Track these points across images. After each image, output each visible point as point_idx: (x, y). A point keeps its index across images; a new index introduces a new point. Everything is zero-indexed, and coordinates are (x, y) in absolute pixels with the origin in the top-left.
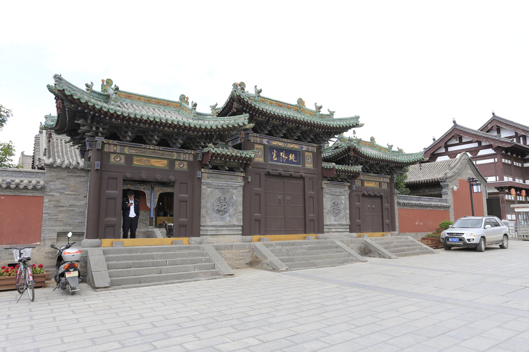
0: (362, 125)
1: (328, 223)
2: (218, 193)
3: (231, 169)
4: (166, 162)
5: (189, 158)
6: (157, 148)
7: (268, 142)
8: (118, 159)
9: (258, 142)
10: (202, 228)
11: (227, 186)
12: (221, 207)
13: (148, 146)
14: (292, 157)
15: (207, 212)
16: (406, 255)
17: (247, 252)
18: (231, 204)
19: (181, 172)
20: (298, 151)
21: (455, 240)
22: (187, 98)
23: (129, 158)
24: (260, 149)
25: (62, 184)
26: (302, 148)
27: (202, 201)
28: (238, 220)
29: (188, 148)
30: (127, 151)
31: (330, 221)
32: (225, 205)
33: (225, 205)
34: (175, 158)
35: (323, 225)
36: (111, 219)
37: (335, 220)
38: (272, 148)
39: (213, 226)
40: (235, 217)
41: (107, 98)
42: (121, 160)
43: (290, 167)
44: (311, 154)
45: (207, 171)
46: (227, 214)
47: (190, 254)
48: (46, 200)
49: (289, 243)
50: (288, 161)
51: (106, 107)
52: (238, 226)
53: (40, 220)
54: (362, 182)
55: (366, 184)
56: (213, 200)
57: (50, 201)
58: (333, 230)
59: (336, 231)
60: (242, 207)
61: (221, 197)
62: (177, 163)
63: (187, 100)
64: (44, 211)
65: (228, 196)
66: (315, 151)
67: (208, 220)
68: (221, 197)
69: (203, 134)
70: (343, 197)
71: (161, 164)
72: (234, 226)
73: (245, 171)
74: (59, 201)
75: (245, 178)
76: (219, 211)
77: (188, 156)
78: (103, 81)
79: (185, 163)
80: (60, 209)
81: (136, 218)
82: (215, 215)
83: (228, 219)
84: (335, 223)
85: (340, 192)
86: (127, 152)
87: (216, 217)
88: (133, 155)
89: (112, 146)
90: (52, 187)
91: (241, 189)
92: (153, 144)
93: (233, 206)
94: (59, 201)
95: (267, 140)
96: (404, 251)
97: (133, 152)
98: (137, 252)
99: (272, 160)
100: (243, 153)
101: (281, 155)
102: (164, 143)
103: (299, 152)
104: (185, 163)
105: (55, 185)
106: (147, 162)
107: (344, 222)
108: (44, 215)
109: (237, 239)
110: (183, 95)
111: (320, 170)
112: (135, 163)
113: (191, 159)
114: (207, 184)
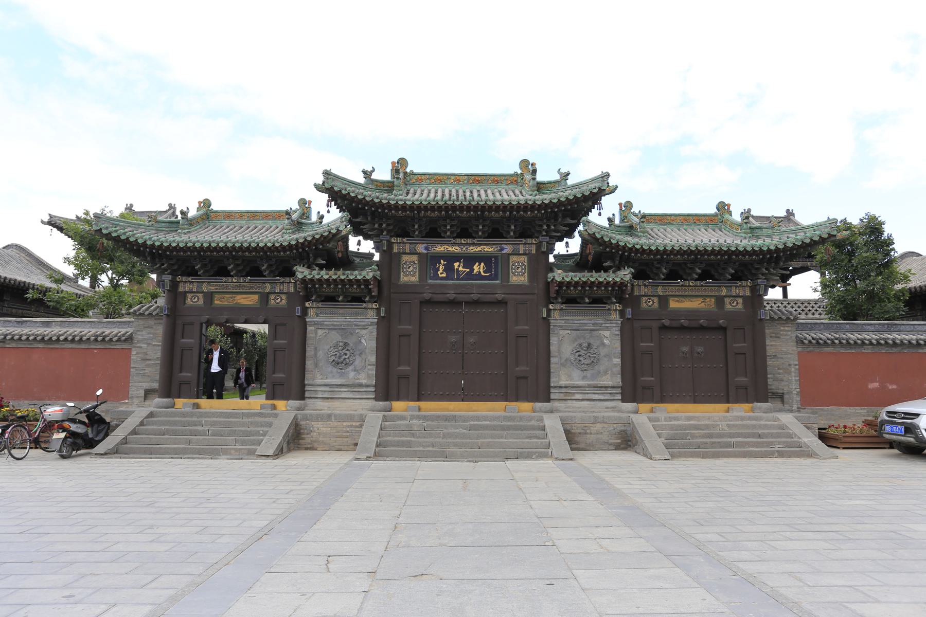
0: (617, 187)
1: (563, 383)
2: (335, 337)
3: (596, 301)
4: (256, 297)
6: (698, 283)
7: (426, 249)
9: (407, 251)
10: (307, 388)
11: (348, 325)
12: (340, 357)
13: (686, 283)
15: (316, 365)
16: (744, 455)
18: (358, 352)
19: (734, 315)
21: (897, 429)
22: (729, 205)
23: (209, 297)
24: (413, 261)
26: (502, 249)
28: (369, 376)
29: (740, 279)
31: (570, 377)
34: (268, 290)
35: (549, 387)
36: (186, 375)
37: (584, 378)
38: (436, 258)
40: (365, 370)
41: (630, 229)
42: (199, 300)
43: (472, 285)
44: (524, 259)
46: (351, 368)
47: (251, 423)
48: (134, 353)
49: (438, 417)
50: (470, 276)
51: (630, 241)
52: (367, 386)
53: (127, 376)
55: (673, 304)
56: (328, 347)
57: (137, 353)
58: (578, 396)
61: (342, 342)
65: (351, 341)
66: (534, 252)
68: (342, 342)
69: (696, 258)
70: (607, 333)
72: (361, 385)
74: (146, 354)
75: (622, 313)
77: (286, 286)
79: (284, 297)
80: (148, 362)
81: (221, 375)
82: (330, 368)
83: (352, 374)
84: (581, 383)
85: (594, 324)
86: (205, 290)
87: (332, 372)
92: (692, 279)
93: (360, 354)
94: (146, 354)
95: (424, 246)
96: (728, 445)
97: (212, 288)
98: (192, 417)
99: (436, 277)
102: (255, 272)
103: (496, 258)
107: (607, 381)
109: (363, 404)
111: (541, 285)
112: (216, 302)
113: (748, 293)
114: (316, 324)
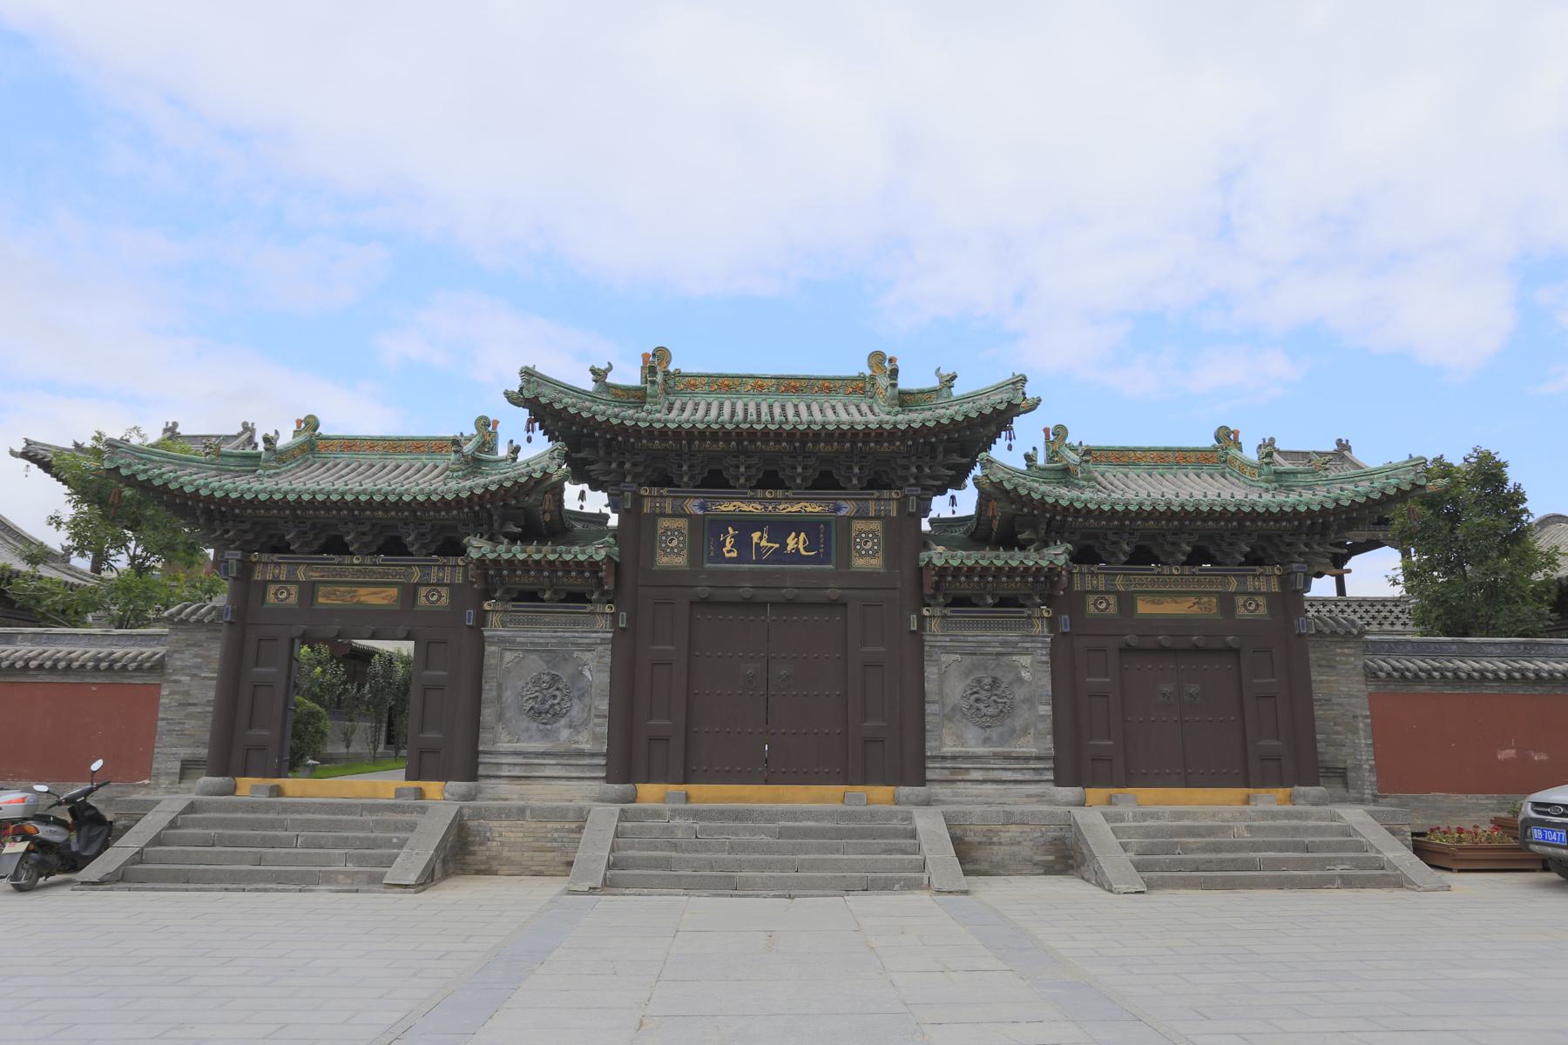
1: (948, 750)
2: (536, 664)
4: (394, 591)
5: (453, 577)
7: (703, 507)
8: (1103, 606)
11: (559, 644)
12: (544, 702)
13: (1166, 570)
14: (795, 542)
17: (571, 831)
18: (576, 693)
22: (1236, 433)
24: (678, 530)
25: (196, 656)
26: (838, 509)
27: (486, 687)
28: (595, 738)
30: (1120, 584)
31: (960, 739)
32: (555, 697)
33: (555, 697)
37: (986, 741)
39: (516, 754)
40: (587, 729)
41: (1064, 474)
42: (290, 597)
45: (938, 611)
46: (563, 722)
47: (377, 823)
48: (165, 692)
49: (722, 812)
51: (1066, 495)
52: (593, 755)
53: (150, 734)
55: (1144, 608)
56: (520, 684)
57: (172, 693)
59: (545, 773)
60: (607, 701)
63: (1236, 438)
64: (161, 715)
65: (565, 673)
66: (894, 513)
67: (504, 737)
68: (550, 677)
70: (1026, 660)
72: (580, 754)
73: (1049, 600)
74: (187, 693)
75: (1053, 624)
76: (536, 714)
77: (449, 572)
78: (1046, 431)
80: (191, 709)
83: (565, 734)
84: (980, 750)
86: (302, 578)
87: (528, 729)
88: (314, 582)
89: (270, 567)
90: (178, 663)
91: (605, 652)
93: (581, 697)
94: (187, 693)
96: (1251, 865)
97: (315, 576)
98: (267, 812)
99: (720, 557)
100: (968, 557)
101: (755, 540)
102: (394, 547)
103: (827, 524)
104: (444, 591)
105: (183, 660)
106: (348, 597)
107: (1026, 746)
108: (160, 723)
110: (481, 418)
112: (321, 600)
113: (1275, 588)
114: (501, 641)
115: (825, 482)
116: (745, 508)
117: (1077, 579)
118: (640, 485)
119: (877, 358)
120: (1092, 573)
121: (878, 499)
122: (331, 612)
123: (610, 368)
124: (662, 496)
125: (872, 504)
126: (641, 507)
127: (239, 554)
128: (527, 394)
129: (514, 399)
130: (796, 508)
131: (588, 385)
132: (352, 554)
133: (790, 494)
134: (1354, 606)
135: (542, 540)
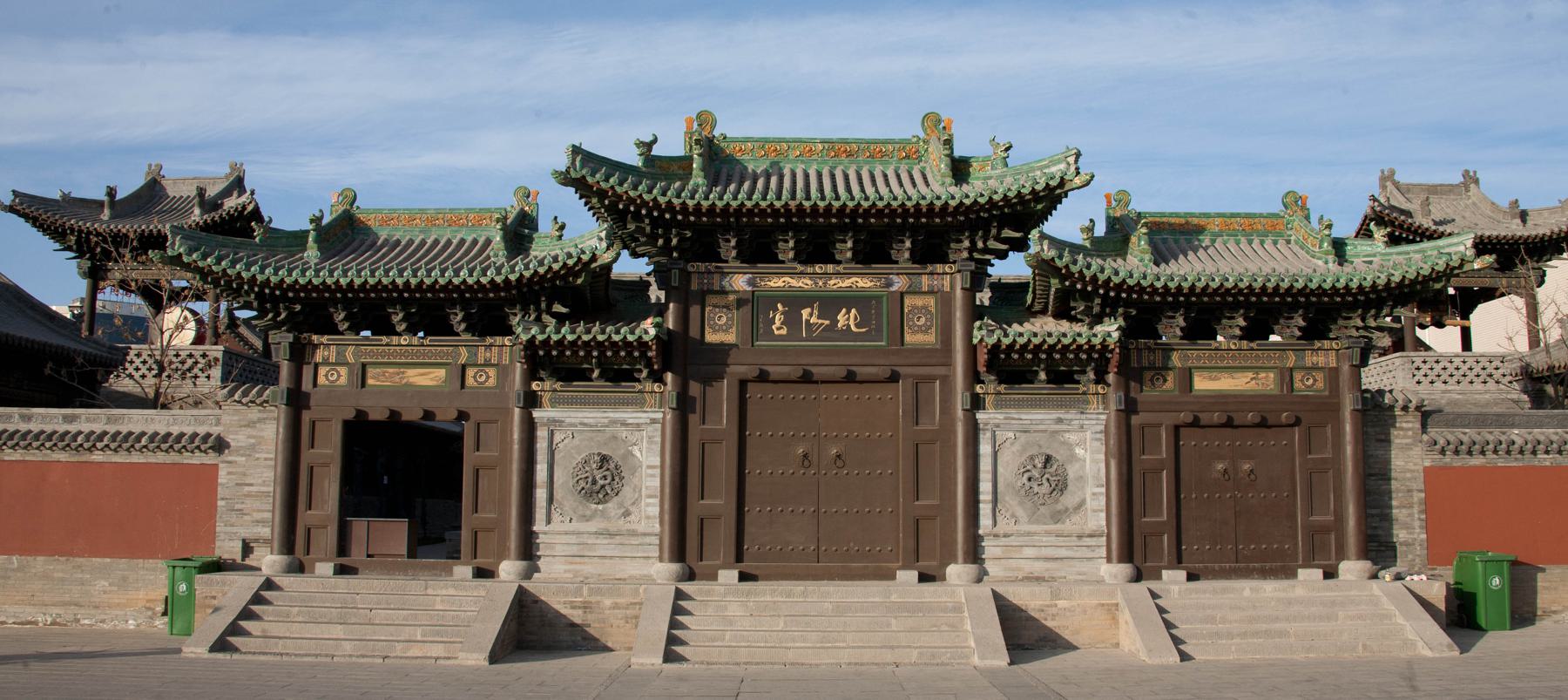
4: (442, 372)
5: (500, 357)
6: (1245, 343)
14: (847, 319)
20: (871, 298)
26: (889, 284)
38: (772, 299)
42: (342, 376)
54: (1187, 377)
55: (1201, 384)
62: (1297, 376)
63: (1304, 204)
71: (429, 378)
78: (1108, 197)
79: (1320, 376)
99: (770, 334)
101: (805, 317)
103: (878, 298)
115: (873, 253)
116: (794, 282)
117: (1134, 356)
118: (688, 261)
119: (932, 121)
120: (1149, 348)
121: (932, 274)
122: (381, 391)
123: (655, 141)
124: (709, 272)
125: (925, 279)
126: (689, 282)
127: (290, 338)
128: (573, 175)
129: (566, 179)
130: (847, 283)
131: (634, 158)
132: (399, 334)
133: (840, 268)
134: (1497, 363)
135: (590, 319)
